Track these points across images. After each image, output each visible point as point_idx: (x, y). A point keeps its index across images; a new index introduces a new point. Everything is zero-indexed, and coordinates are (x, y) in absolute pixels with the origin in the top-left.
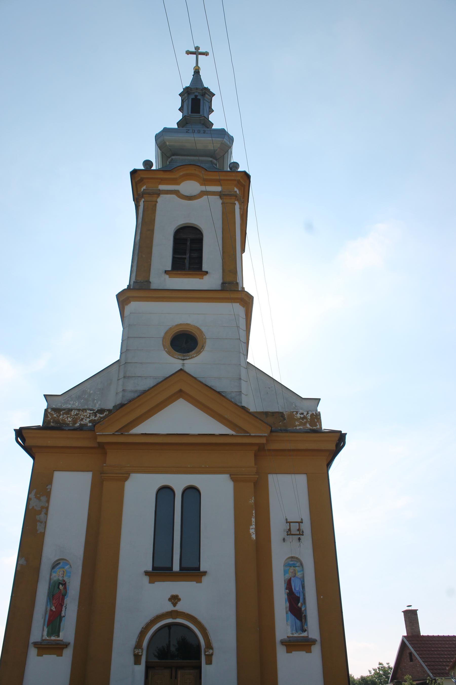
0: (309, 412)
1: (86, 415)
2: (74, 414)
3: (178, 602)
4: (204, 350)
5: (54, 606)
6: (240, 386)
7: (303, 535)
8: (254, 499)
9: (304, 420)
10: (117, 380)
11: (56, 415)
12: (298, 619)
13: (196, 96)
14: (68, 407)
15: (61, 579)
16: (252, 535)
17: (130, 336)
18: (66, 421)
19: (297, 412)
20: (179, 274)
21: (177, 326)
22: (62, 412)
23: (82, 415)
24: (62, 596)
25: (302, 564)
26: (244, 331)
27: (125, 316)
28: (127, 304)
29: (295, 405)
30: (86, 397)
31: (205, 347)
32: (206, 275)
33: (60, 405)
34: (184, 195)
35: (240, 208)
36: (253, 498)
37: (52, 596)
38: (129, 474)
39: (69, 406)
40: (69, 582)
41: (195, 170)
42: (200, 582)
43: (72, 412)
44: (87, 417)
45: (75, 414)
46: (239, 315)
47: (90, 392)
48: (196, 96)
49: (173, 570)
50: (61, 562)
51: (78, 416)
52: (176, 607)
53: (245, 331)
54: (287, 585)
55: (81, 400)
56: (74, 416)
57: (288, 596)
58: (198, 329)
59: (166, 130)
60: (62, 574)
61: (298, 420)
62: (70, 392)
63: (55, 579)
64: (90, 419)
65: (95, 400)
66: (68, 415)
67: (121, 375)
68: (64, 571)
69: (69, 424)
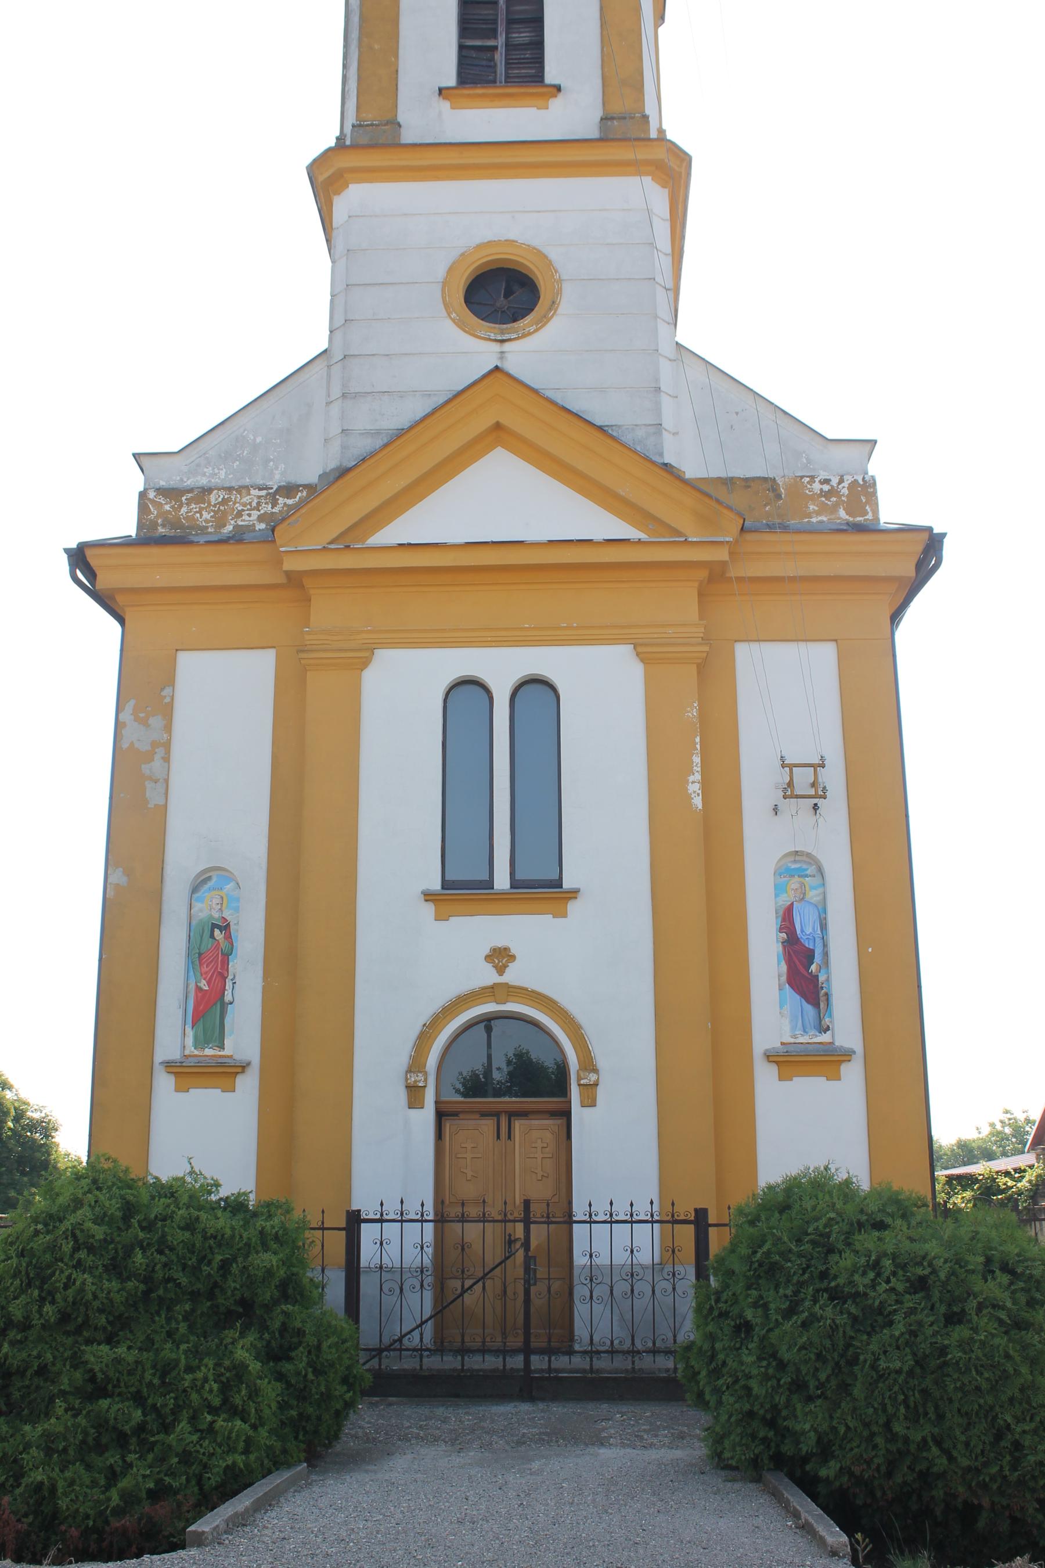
2: (217, 499)
5: (204, 979)
6: (657, 410)
9: (832, 500)
12: (808, 1002)
15: (216, 915)
16: (693, 799)
19: (812, 478)
21: (480, 247)
22: (185, 497)
25: (820, 870)
30: (244, 454)
33: (178, 478)
36: (695, 705)
39: (203, 481)
43: (211, 496)
44: (251, 506)
45: (220, 500)
47: (255, 440)
51: (227, 505)
53: (669, 254)
54: (784, 920)
55: (233, 463)
57: (784, 947)
61: (813, 498)
62: (203, 445)
63: (202, 915)
64: (259, 513)
66: (202, 505)
67: (336, 392)
69: (207, 527)
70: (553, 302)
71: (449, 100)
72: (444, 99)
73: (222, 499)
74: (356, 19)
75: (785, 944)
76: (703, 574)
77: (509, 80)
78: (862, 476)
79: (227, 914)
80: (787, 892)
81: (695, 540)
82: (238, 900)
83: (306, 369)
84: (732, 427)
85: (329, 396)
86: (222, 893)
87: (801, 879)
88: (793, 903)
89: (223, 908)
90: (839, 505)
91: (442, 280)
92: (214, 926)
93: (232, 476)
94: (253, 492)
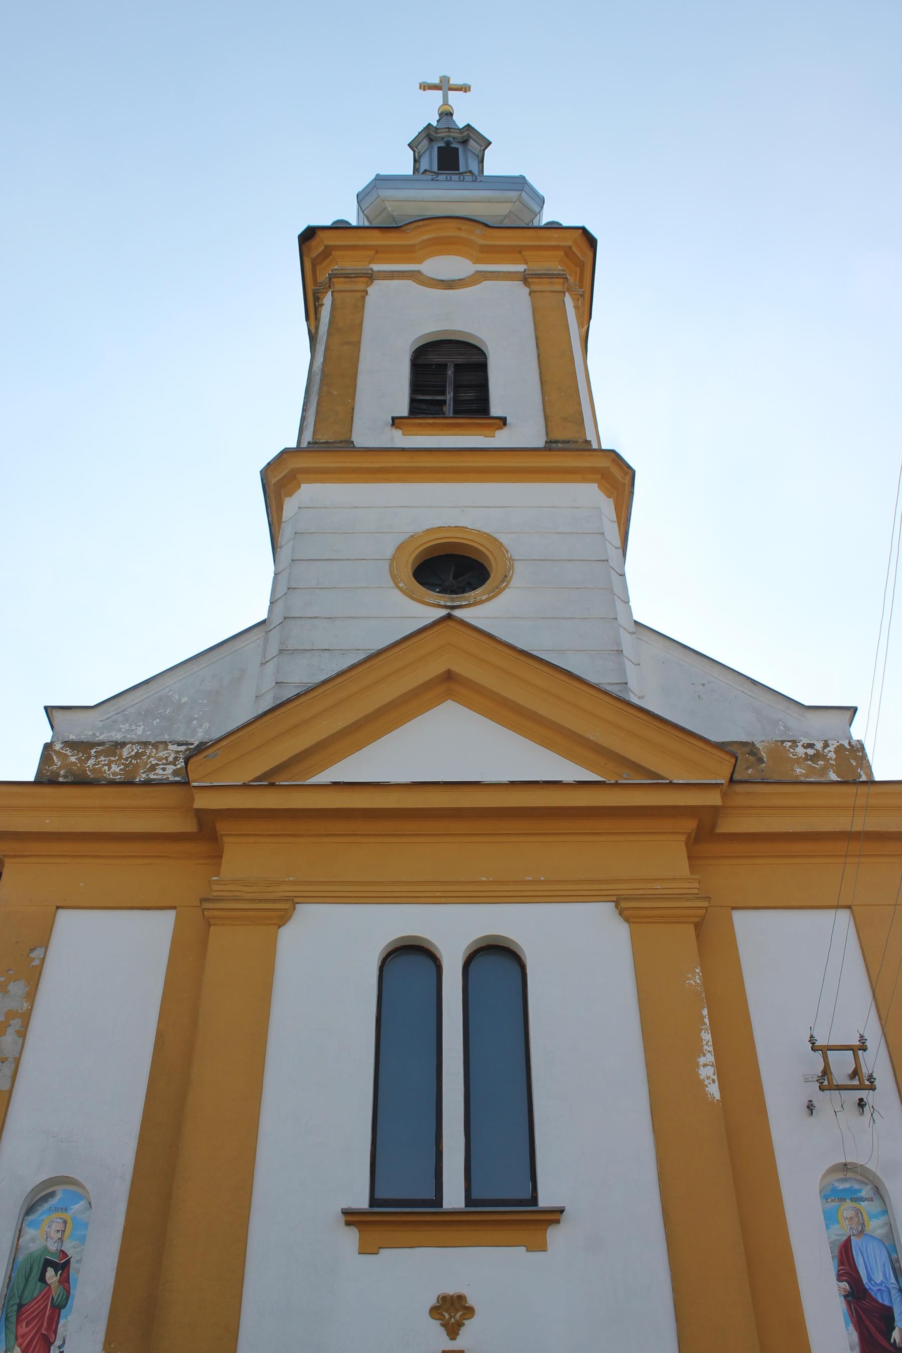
0: (830, 742)
1: (164, 756)
3: (465, 1322)
4: (511, 585)
5: (20, 1346)
6: (622, 671)
7: (873, 1088)
8: (701, 974)
9: (819, 763)
10: (260, 665)
11: (75, 757)
13: (448, 143)
14: (114, 739)
16: (707, 1086)
17: (296, 558)
18: (105, 772)
19: (794, 743)
20: (430, 425)
21: (429, 531)
22: (95, 750)
23: (153, 757)
24: (53, 1306)
25: (879, 1192)
26: (616, 548)
27: (284, 519)
28: (290, 494)
29: (784, 727)
30: (167, 712)
31: (513, 579)
32: (502, 429)
33: (91, 733)
34: (432, 279)
35: (576, 307)
36: (698, 971)
37: (15, 1308)
38: (293, 902)
39: (118, 737)
40: (78, 1259)
41: (460, 229)
42: (542, 1247)
43: (124, 750)
45: (133, 753)
46: (600, 508)
47: (180, 700)
48: (448, 143)
49: (444, 1207)
50: (60, 1190)
51: (140, 759)
52: (458, 1337)
53: (619, 548)
54: (841, 1263)
55: (153, 720)
56: (130, 759)
57: (849, 1303)
58: (489, 537)
59: (380, 181)
60: (58, 1231)
61: (799, 761)
62: (122, 702)
64: (175, 768)
65: (195, 719)
66: (113, 759)
67: (273, 650)
68: (65, 1222)
70: (505, 576)
71: (401, 429)
72: (396, 428)
73: (136, 753)
74: (317, 379)
75: (850, 1298)
76: (691, 825)
77: (458, 412)
78: (848, 741)
79: (68, 1248)
80: (839, 1223)
81: (681, 782)
82: (86, 1226)
83: (242, 638)
84: (699, 697)
85: (264, 658)
86: (67, 1216)
87: (854, 1204)
88: (850, 1237)
89: (65, 1238)
90: (828, 768)
91: (390, 558)
92: (48, 1263)
93: (150, 732)
94: (171, 747)
